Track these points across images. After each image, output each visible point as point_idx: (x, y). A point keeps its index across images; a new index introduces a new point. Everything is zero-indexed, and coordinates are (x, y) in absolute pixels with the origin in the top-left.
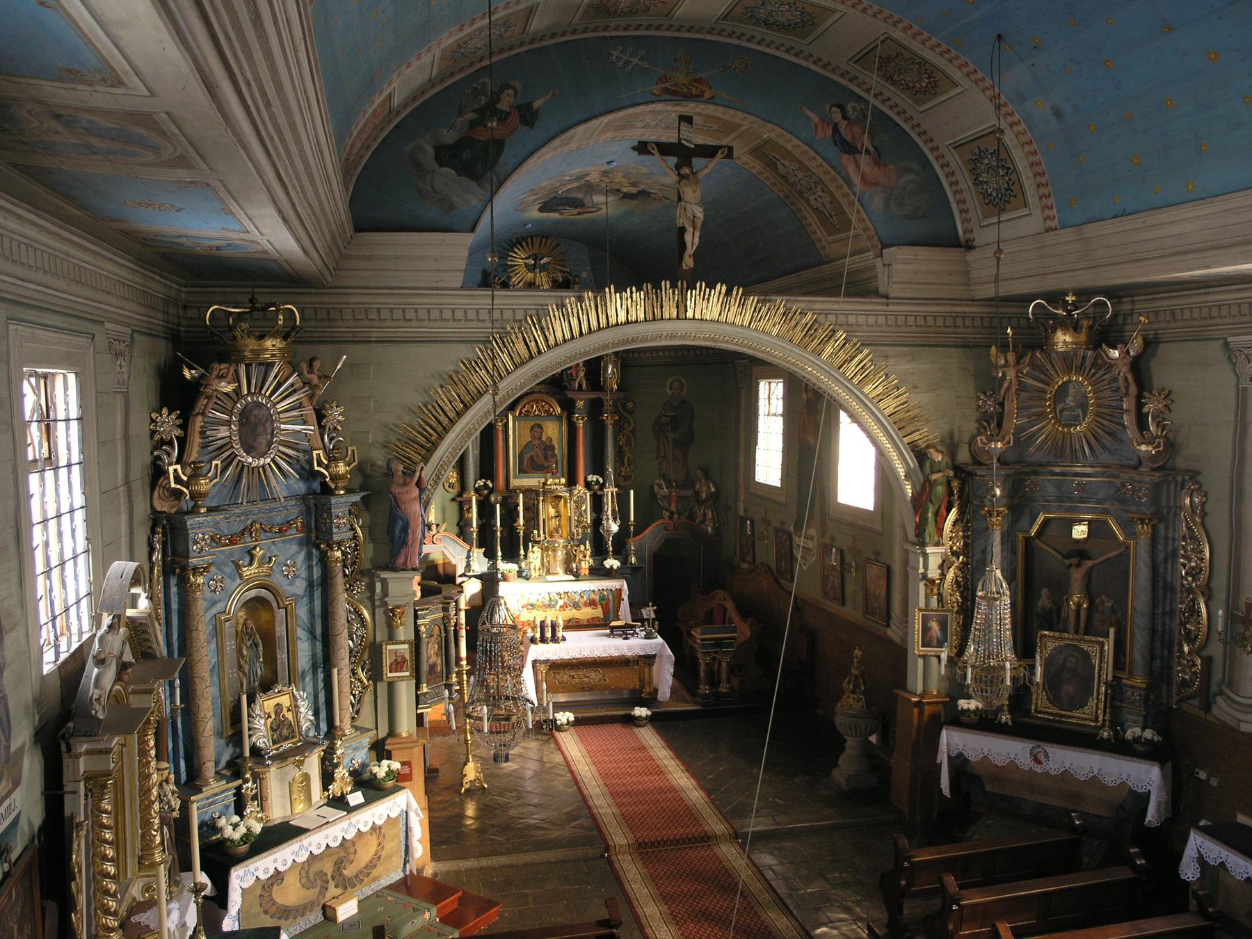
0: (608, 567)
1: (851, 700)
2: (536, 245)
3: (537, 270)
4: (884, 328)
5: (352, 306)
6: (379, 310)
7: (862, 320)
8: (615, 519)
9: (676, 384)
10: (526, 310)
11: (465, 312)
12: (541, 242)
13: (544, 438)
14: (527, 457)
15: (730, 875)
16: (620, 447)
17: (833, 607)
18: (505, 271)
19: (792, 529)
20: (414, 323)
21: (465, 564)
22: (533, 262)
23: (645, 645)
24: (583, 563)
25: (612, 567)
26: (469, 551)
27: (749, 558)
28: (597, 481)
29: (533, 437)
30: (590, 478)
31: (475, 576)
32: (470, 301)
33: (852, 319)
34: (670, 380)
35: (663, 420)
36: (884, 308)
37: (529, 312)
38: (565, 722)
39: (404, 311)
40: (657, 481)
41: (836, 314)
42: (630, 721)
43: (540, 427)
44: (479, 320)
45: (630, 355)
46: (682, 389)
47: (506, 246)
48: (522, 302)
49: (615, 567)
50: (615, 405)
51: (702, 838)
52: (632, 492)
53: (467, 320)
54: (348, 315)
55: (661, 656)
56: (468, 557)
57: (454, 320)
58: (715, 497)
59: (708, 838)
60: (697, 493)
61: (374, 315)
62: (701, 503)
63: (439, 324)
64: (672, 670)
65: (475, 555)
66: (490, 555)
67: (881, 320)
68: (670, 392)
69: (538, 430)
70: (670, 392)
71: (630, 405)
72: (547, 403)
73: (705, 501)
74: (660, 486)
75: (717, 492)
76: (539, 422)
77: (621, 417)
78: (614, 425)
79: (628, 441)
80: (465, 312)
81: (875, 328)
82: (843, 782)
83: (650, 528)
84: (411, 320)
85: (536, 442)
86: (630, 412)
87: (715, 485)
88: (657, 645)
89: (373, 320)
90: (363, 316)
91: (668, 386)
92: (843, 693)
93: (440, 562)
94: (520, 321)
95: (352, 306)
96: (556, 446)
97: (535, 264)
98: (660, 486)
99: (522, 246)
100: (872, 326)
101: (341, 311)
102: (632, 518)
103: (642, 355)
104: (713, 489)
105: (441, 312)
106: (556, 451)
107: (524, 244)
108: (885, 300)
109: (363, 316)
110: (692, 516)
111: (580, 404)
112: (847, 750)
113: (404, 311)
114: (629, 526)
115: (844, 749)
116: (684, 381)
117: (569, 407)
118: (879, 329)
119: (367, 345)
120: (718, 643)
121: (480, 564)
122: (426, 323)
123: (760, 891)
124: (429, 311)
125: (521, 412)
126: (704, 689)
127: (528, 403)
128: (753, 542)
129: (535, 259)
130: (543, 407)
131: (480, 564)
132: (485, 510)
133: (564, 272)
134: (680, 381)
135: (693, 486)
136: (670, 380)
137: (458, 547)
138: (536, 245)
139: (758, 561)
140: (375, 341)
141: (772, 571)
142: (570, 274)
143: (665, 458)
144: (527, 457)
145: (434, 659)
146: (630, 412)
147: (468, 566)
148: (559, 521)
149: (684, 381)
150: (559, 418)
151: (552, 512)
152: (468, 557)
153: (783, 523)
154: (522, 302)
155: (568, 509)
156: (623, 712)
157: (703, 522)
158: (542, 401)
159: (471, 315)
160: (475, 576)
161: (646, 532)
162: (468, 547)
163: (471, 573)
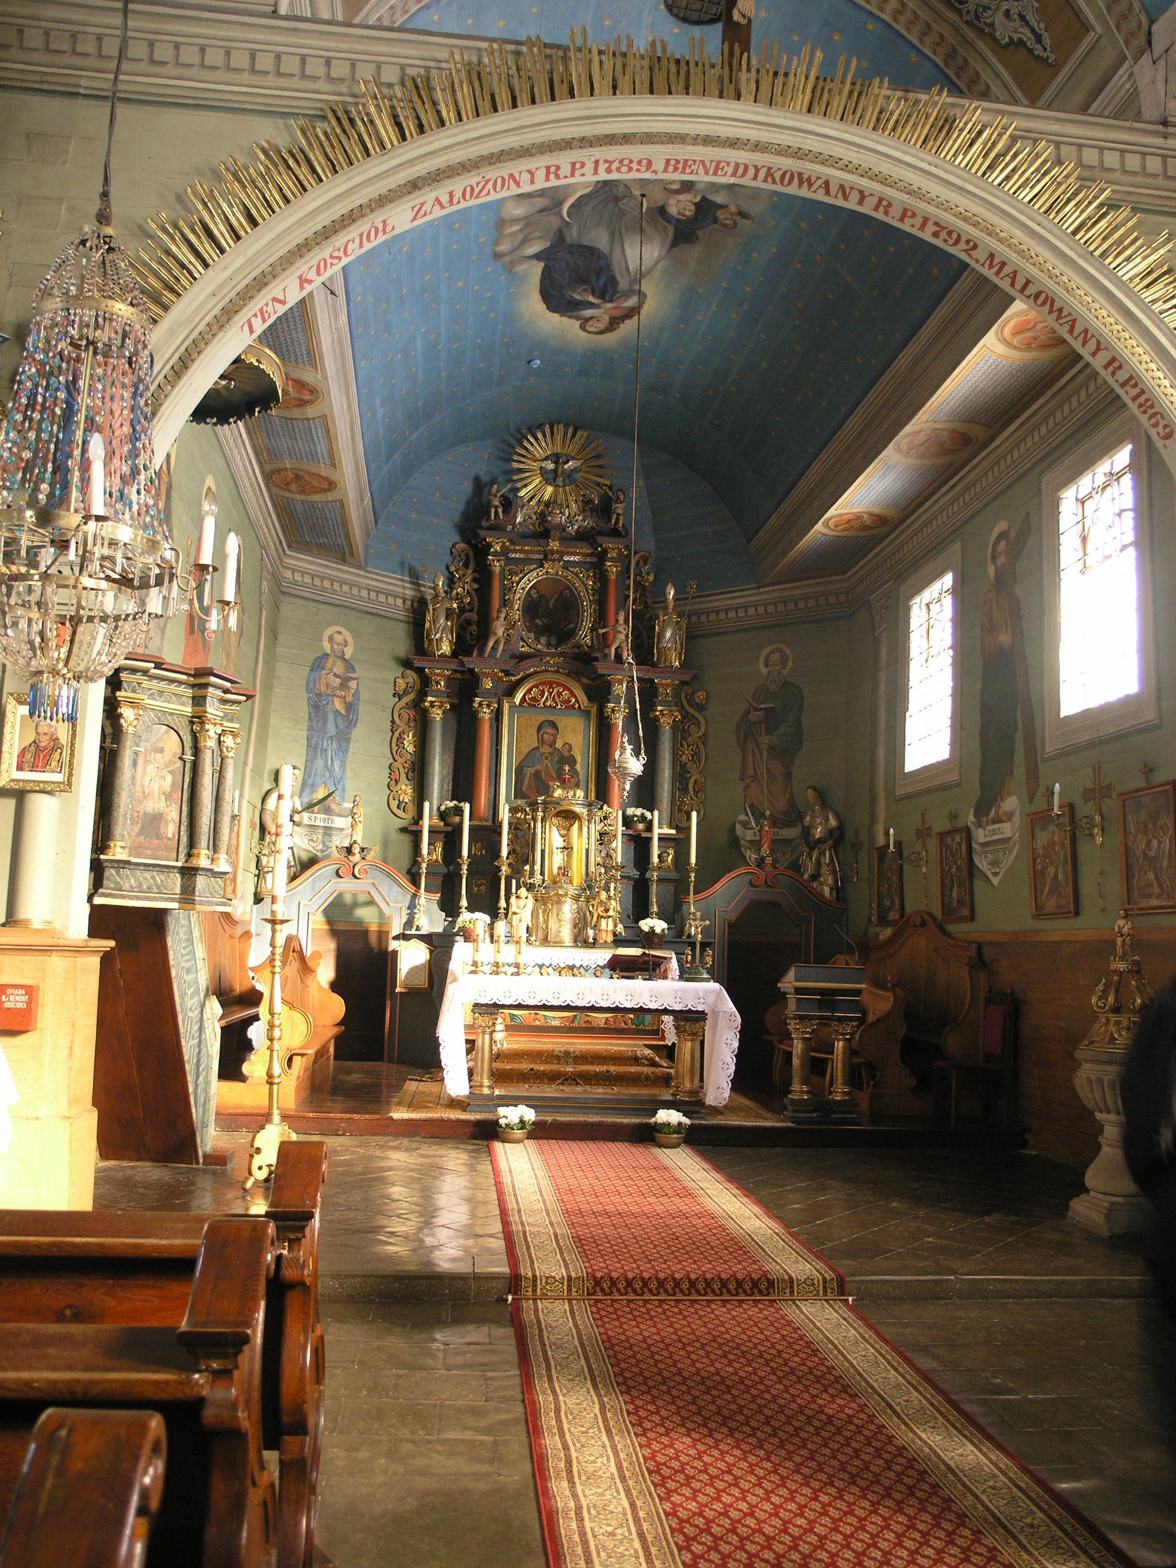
0: (646, 929)
1: (1113, 1028)
2: (559, 438)
3: (560, 481)
4: (1160, 181)
5: (44, 24)
6: (99, 38)
7: (1112, 159)
8: (637, 753)
9: (776, 657)
10: (403, 67)
11: (278, 57)
12: (566, 434)
13: (559, 745)
14: (529, 772)
15: (815, 1352)
16: (683, 766)
17: (1057, 929)
18: (511, 481)
19: (971, 818)
20: (170, 70)
21: (405, 918)
22: (551, 466)
23: (684, 991)
24: (603, 921)
25: (652, 928)
26: (414, 896)
27: (893, 916)
28: (643, 817)
29: (542, 741)
30: (630, 811)
31: (422, 938)
32: (290, 40)
33: (1091, 157)
34: (766, 651)
35: (754, 716)
36: (1159, 141)
37: (411, 72)
38: (517, 1121)
39: (151, 44)
40: (742, 817)
41: (1101, 149)
42: (647, 1135)
43: (554, 725)
44: (304, 76)
45: (703, 618)
46: (784, 664)
47: (512, 441)
48: (396, 50)
49: (658, 930)
50: (677, 695)
51: (755, 1284)
52: (694, 814)
53: (279, 74)
54: (34, 38)
55: (716, 1013)
56: (412, 907)
57: (253, 70)
58: (837, 837)
59: (771, 1284)
60: (807, 832)
61: (89, 47)
62: (813, 845)
63: (221, 75)
64: (736, 1044)
65: (422, 901)
66: (449, 907)
67: (1154, 165)
68: (764, 671)
69: (551, 731)
70: (764, 671)
71: (700, 696)
72: (566, 688)
73: (819, 841)
74: (745, 825)
75: (841, 828)
76: (551, 718)
77: (685, 715)
78: (675, 727)
79: (695, 757)
80: (278, 57)
81: (1139, 179)
82: (1099, 1219)
83: (724, 881)
84: (165, 63)
85: (546, 749)
86: (701, 708)
87: (837, 816)
88: (707, 992)
89: (87, 55)
90: (65, 46)
91: (762, 661)
92: (1095, 1016)
93: (374, 928)
94: (390, 86)
95: (44, 24)
96: (579, 759)
97: (555, 471)
98: (745, 825)
99: (536, 439)
100: (1135, 173)
101: (21, 32)
102: (693, 860)
103: (722, 616)
104: (833, 822)
105: (228, 53)
106: (578, 767)
107: (540, 436)
108: (1161, 128)
109: (65, 46)
110: (796, 867)
111: (620, 689)
112: (1105, 1149)
113: (151, 44)
114: (688, 872)
115: (1099, 1147)
116: (788, 651)
117: (600, 693)
118: (1149, 181)
119: (67, 102)
120: (827, 999)
121: (430, 919)
122: (194, 72)
123: (898, 1386)
124: (203, 50)
125: (523, 699)
126: (799, 1090)
127: (536, 686)
128: (901, 867)
129: (556, 463)
130: (559, 694)
131: (431, 921)
132: (449, 838)
133: (598, 484)
134: (781, 651)
135: (801, 818)
136: (766, 651)
137: (396, 888)
138: (559, 438)
139: (909, 909)
140: (84, 96)
141: (934, 918)
142: (610, 488)
143: (755, 777)
144: (529, 772)
145: (157, 804)
146: (701, 708)
147: (409, 923)
148: (569, 856)
149: (788, 651)
150: (587, 713)
151: (557, 840)
152: (412, 907)
153: (953, 817)
154: (396, 50)
155: (583, 838)
156: (636, 1120)
157: (815, 877)
158: (559, 685)
159: (290, 65)
160: (422, 938)
161: (718, 886)
162: (412, 889)
163: (413, 932)
